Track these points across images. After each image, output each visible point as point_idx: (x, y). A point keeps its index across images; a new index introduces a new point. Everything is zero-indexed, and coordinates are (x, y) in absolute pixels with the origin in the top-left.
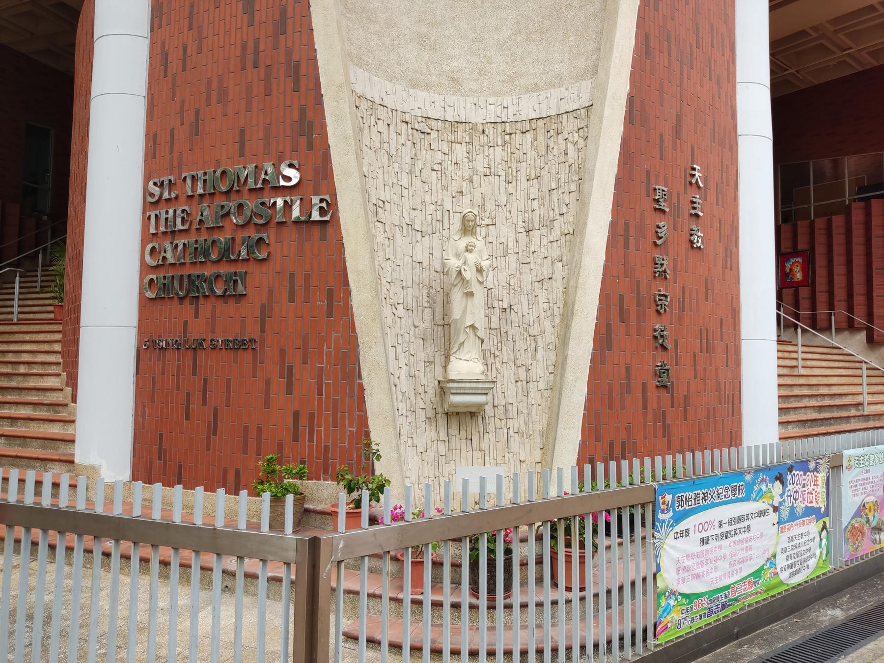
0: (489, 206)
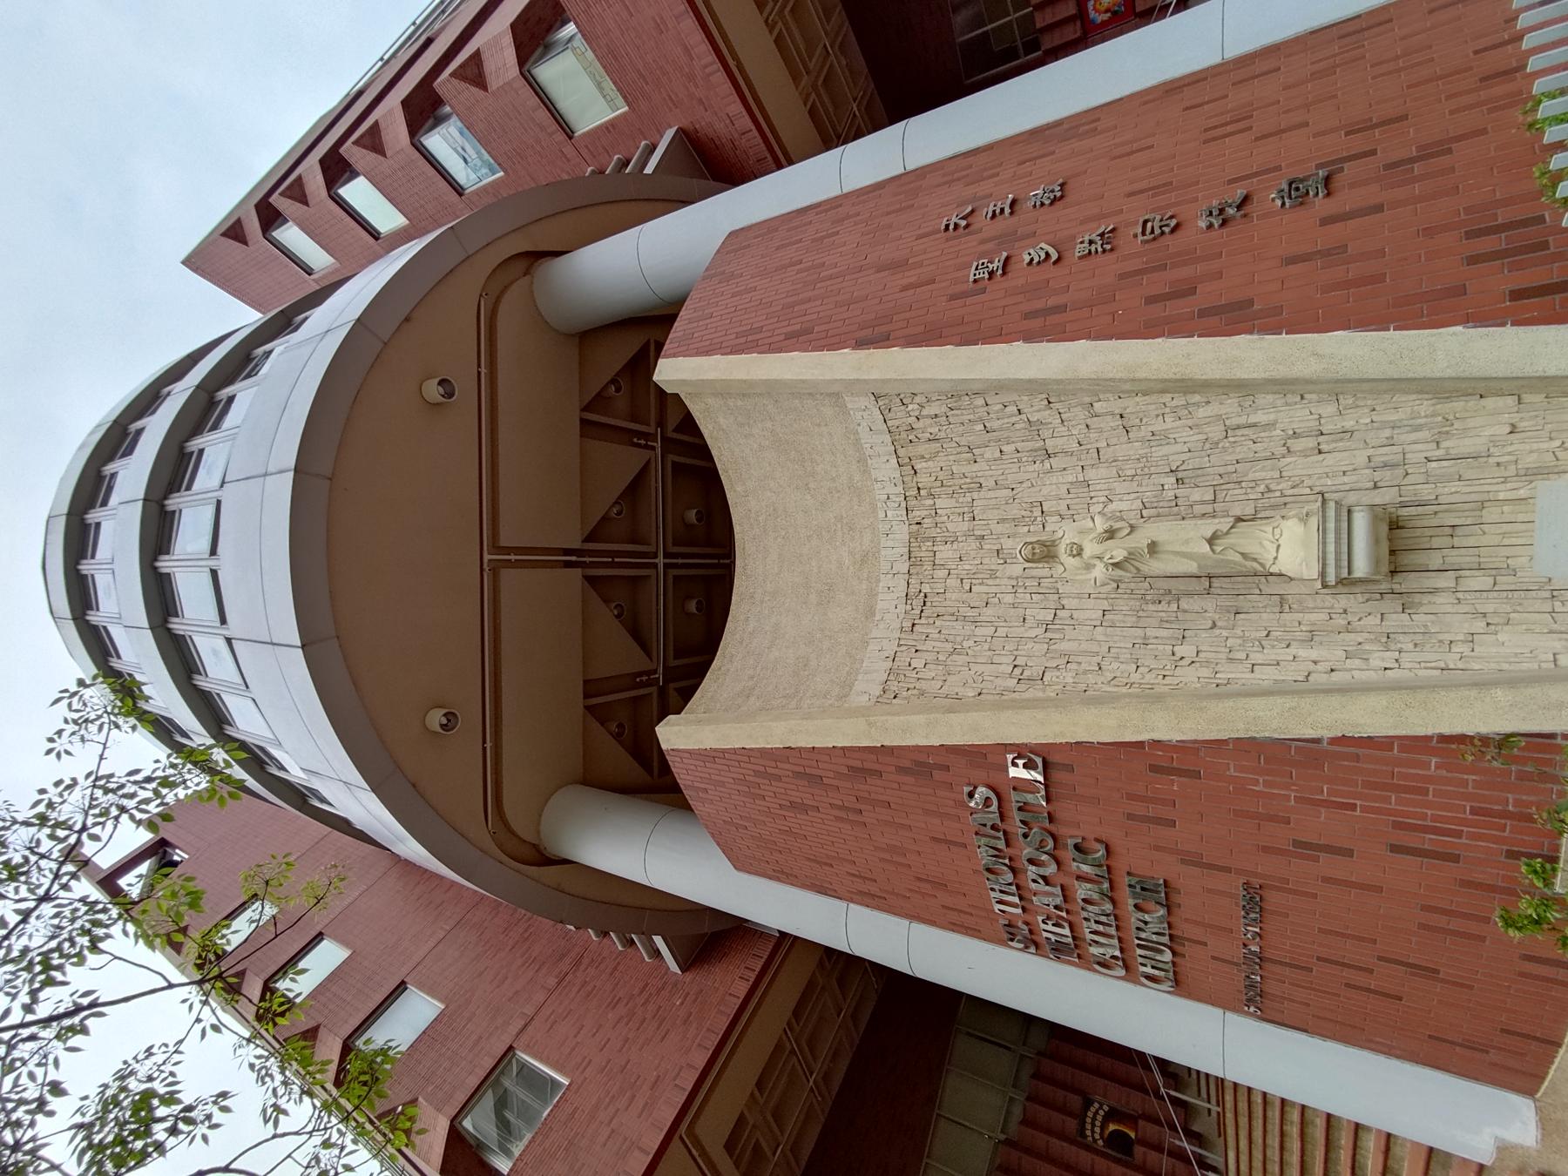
0: (1015, 511)
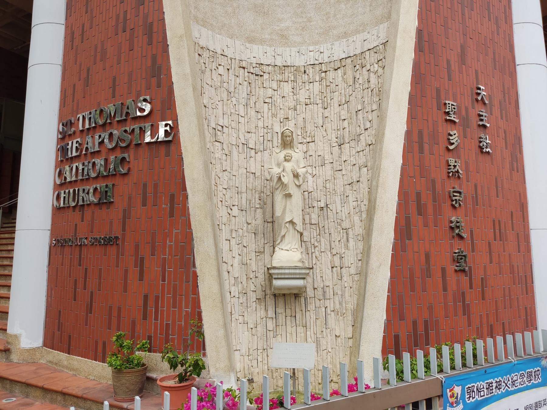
0: (310, 128)
